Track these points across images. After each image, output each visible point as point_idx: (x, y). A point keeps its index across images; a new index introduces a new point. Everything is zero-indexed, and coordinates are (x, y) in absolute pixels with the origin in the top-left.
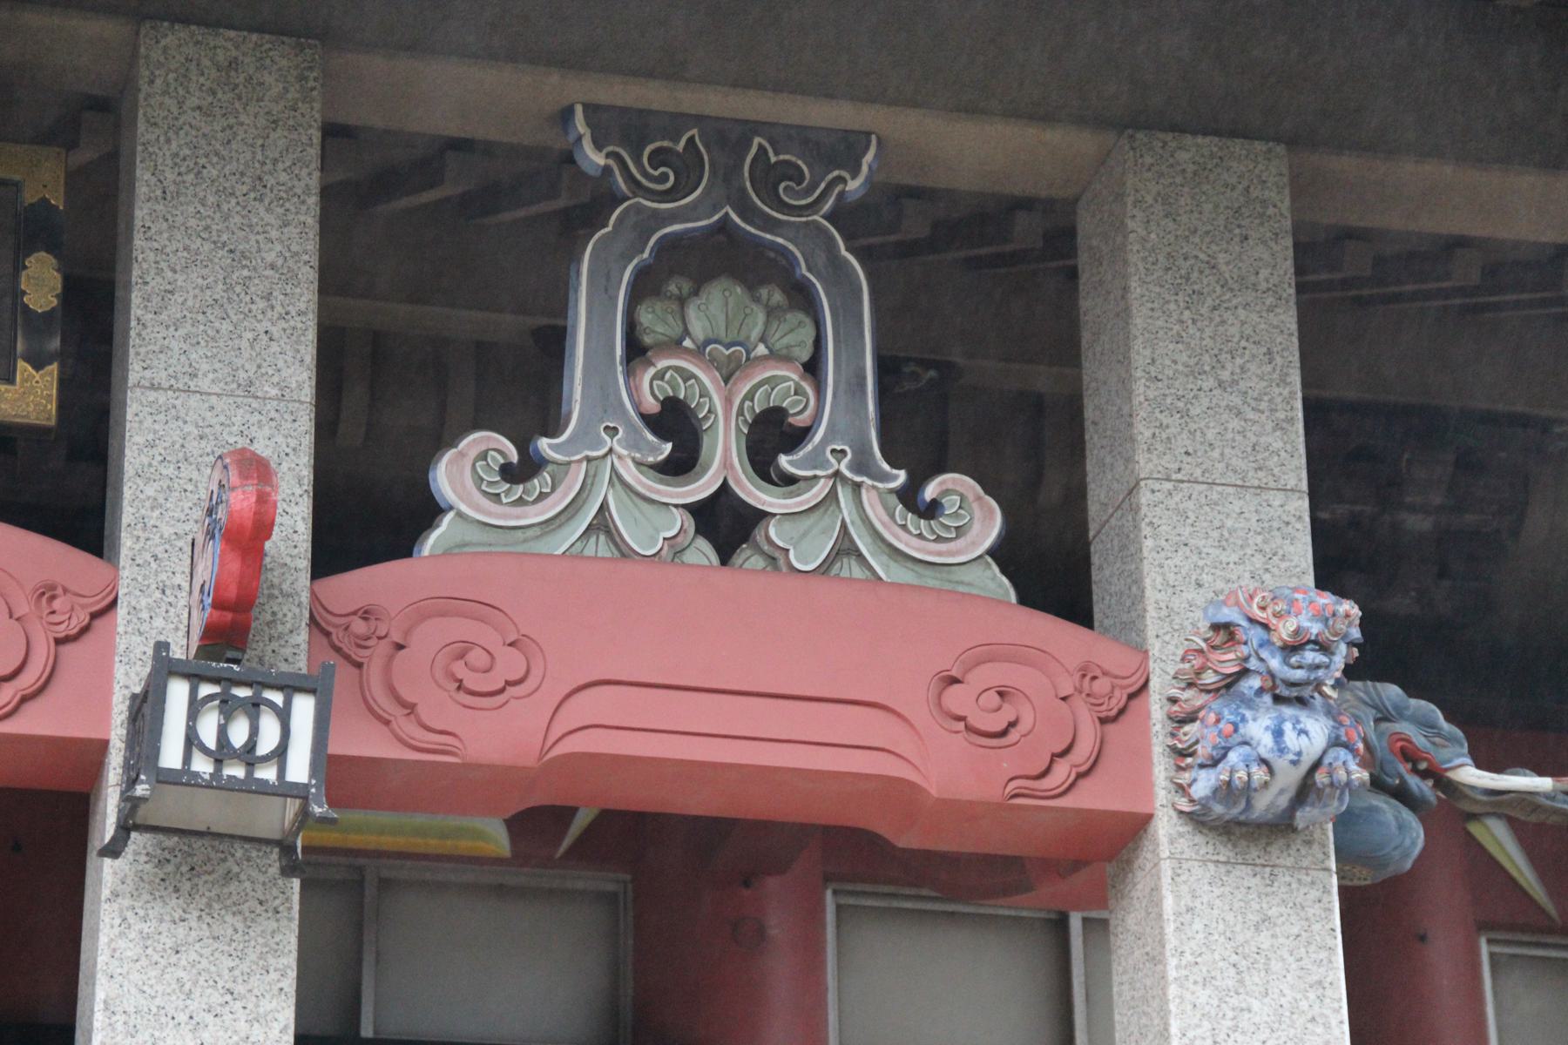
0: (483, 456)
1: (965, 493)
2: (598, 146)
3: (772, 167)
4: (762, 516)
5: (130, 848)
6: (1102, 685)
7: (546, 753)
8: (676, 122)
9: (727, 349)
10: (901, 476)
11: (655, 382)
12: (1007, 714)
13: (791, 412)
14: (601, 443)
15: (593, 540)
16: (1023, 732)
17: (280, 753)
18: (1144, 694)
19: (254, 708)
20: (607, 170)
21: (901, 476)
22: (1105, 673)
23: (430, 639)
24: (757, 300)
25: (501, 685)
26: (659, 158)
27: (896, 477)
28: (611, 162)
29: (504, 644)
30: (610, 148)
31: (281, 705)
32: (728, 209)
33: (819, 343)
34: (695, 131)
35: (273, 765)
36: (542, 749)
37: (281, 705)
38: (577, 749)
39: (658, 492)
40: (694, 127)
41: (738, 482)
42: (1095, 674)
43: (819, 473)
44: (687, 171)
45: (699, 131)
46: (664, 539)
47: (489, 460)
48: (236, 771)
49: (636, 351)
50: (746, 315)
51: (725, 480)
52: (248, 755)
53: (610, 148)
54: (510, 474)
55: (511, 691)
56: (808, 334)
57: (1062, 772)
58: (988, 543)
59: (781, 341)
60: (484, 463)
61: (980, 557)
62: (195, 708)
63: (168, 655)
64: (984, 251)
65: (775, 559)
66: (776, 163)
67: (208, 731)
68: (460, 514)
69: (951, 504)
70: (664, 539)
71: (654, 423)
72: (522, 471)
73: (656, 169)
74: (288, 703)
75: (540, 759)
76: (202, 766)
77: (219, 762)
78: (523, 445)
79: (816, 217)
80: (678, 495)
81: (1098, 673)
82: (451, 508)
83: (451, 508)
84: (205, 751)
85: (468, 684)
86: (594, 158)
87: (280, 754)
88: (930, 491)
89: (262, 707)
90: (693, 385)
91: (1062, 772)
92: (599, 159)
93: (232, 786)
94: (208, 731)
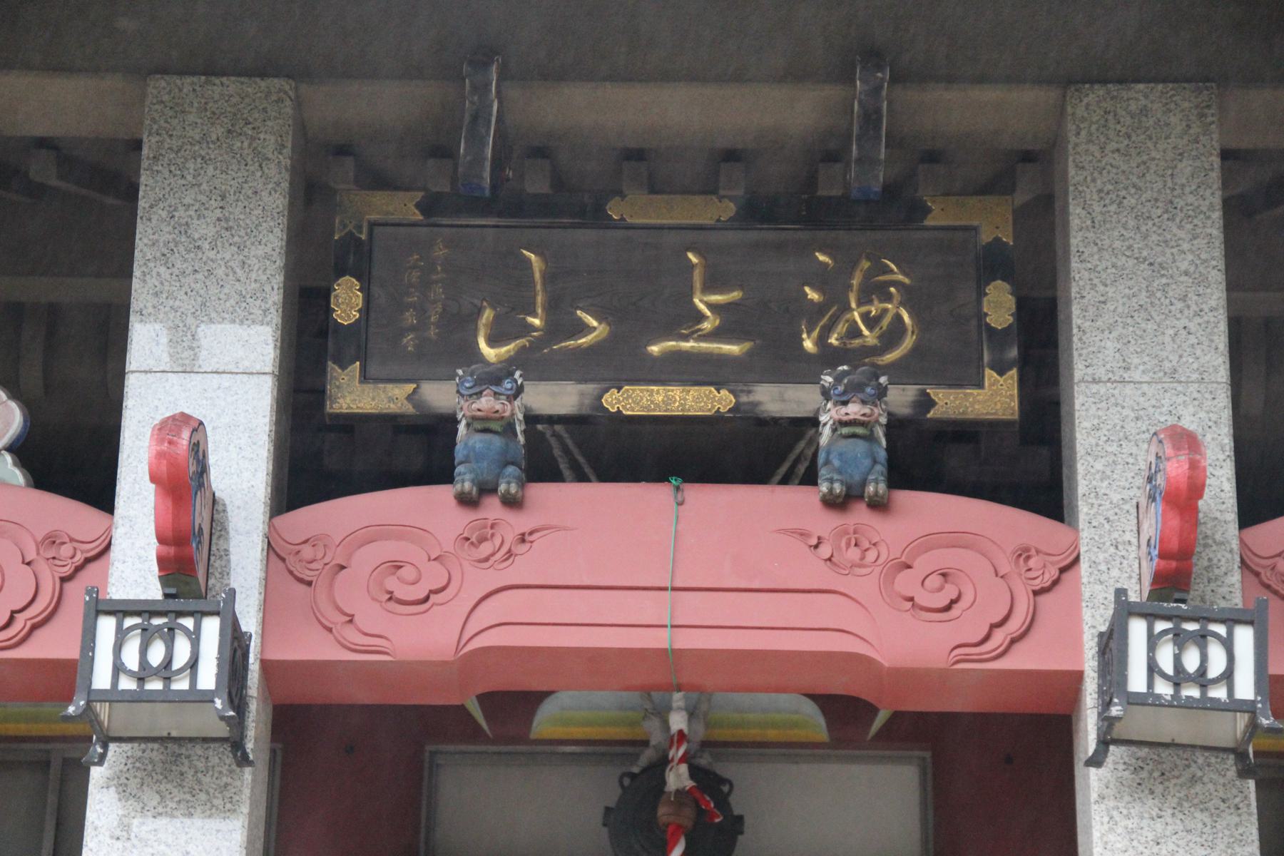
23: (367, 559)
52: (1200, 677)
57: (999, 637)
67: (1165, 658)
76: (1164, 689)
87: (1228, 676)
91: (999, 637)
94: (131, 658)
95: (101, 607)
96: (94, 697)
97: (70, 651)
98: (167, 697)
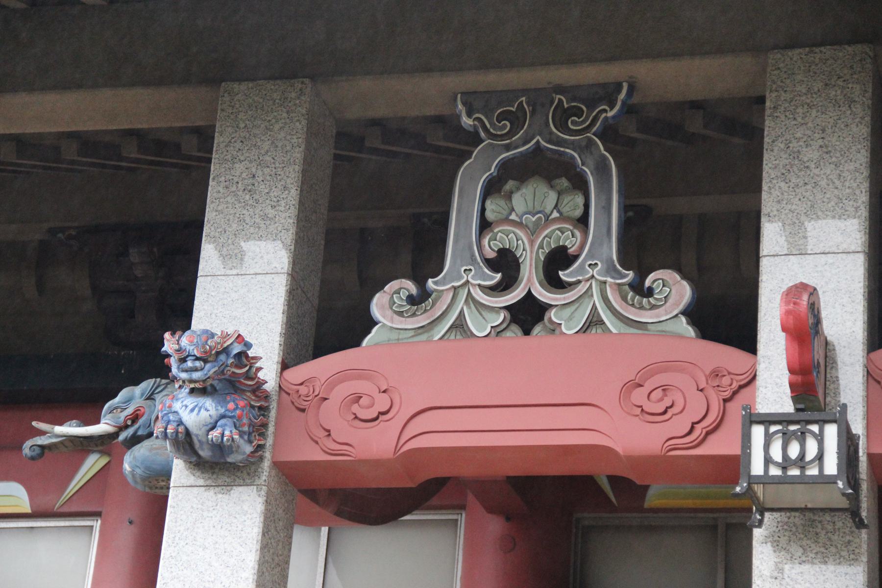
0: (398, 292)
1: (664, 278)
2: (469, 115)
3: (565, 111)
4: (545, 307)
5: (766, 520)
6: (726, 381)
7: (399, 450)
8: (511, 95)
9: (533, 217)
10: (631, 275)
11: (491, 243)
12: (667, 402)
13: (569, 247)
14: (461, 277)
15: (454, 333)
16: (675, 413)
17: (820, 457)
18: (752, 384)
19: (802, 438)
20: (475, 126)
21: (631, 275)
22: (729, 373)
24: (552, 187)
25: (375, 415)
26: (502, 117)
27: (628, 275)
28: (476, 123)
29: (379, 392)
30: (477, 115)
31: (817, 432)
32: (538, 138)
33: (587, 206)
34: (524, 99)
35: (814, 467)
36: (395, 450)
37: (817, 432)
38: (410, 448)
39: (569, 298)
40: (522, 96)
41: (536, 289)
42: (724, 374)
43: (580, 278)
44: (516, 120)
45: (526, 99)
46: (492, 327)
47: (401, 293)
48: (795, 472)
49: (485, 225)
50: (545, 197)
51: (529, 289)
53: (477, 115)
54: (412, 300)
55: (382, 418)
56: (580, 200)
58: (681, 307)
59: (566, 210)
60: (398, 295)
61: (676, 316)
62: (768, 439)
63: (750, 412)
64: (48, 164)
65: (554, 329)
66: (568, 108)
68: (384, 325)
69: (657, 287)
70: (492, 327)
71: (493, 264)
72: (418, 300)
73: (500, 123)
74: (821, 431)
75: (395, 453)
77: (784, 468)
78: (421, 282)
79: (588, 135)
80: (501, 302)
81: (726, 373)
82: (380, 322)
83: (380, 322)
84: (777, 464)
85: (359, 416)
86: (467, 122)
88: (647, 283)
89: (807, 434)
90: (501, 236)
92: (470, 122)
93: (793, 481)
94: (776, 453)
95: (753, 419)
96: (753, 480)
97: (735, 449)
98: (803, 480)
